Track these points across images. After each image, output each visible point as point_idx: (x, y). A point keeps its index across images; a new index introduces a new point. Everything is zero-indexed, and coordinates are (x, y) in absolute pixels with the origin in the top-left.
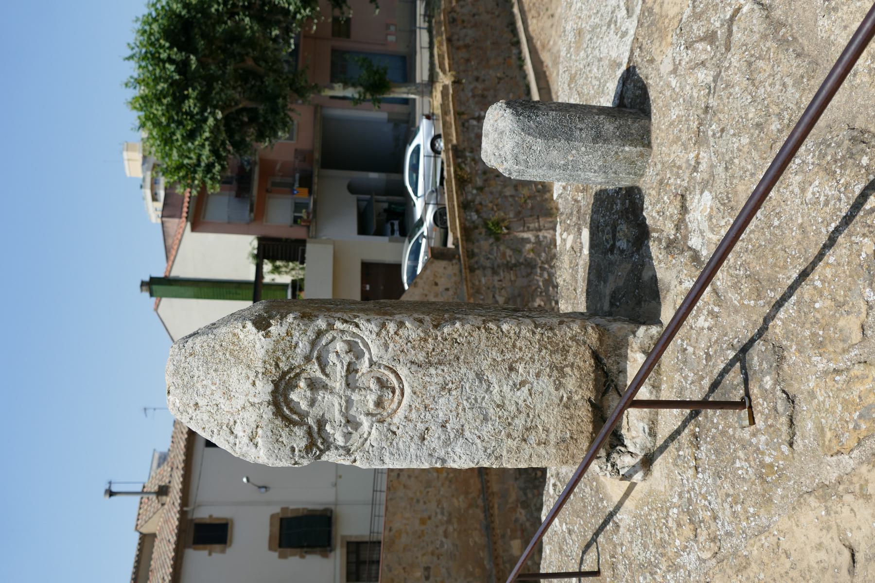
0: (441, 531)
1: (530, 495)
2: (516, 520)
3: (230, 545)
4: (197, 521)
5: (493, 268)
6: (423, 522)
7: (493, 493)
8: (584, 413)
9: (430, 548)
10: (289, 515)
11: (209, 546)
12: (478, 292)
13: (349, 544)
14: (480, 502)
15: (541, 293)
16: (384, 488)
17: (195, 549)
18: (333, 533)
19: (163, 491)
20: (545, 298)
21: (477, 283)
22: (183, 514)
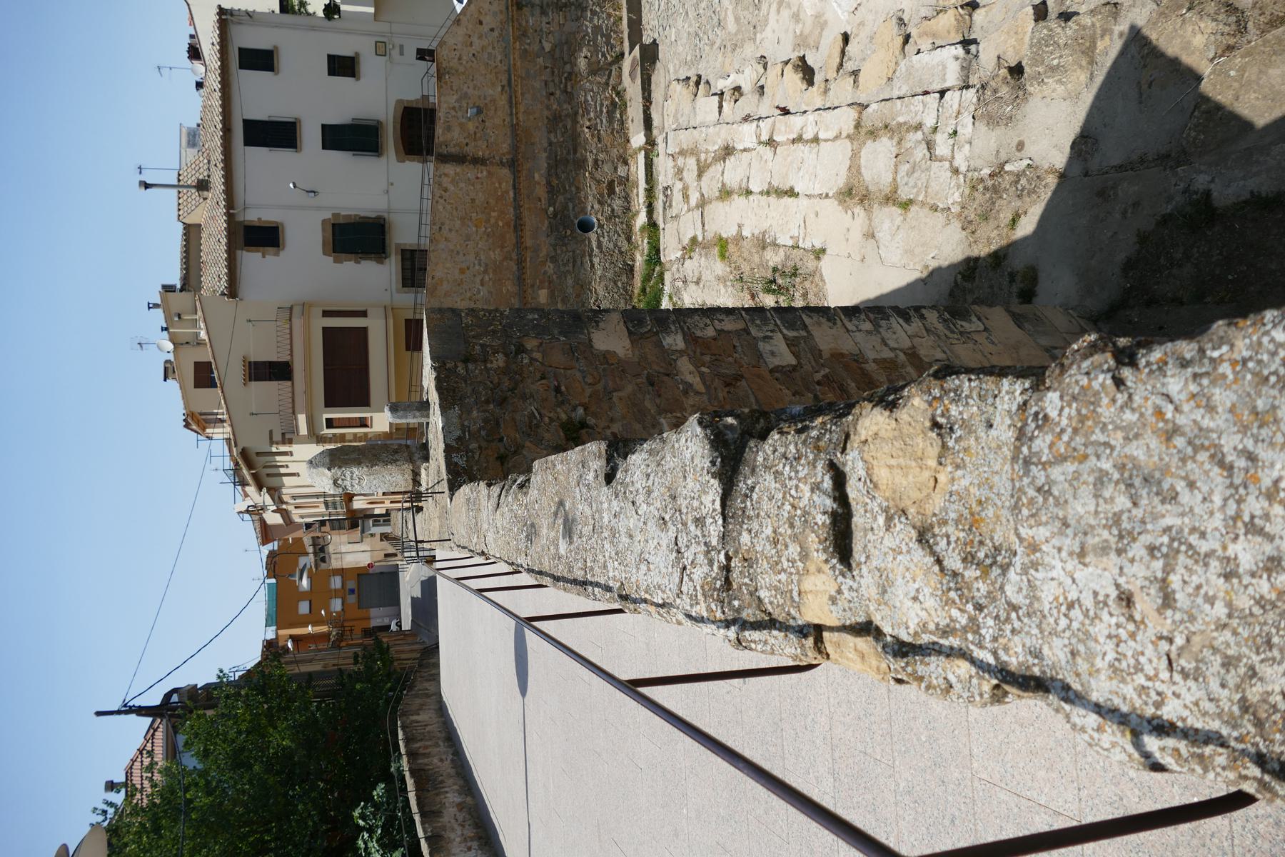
0: (478, 280)
1: (559, 252)
2: (545, 272)
3: (283, 249)
4: (246, 223)
5: (542, 7)
6: (462, 271)
7: (526, 248)
8: (411, 481)
9: (469, 294)
10: (341, 221)
11: (261, 249)
12: (524, 34)
13: (403, 251)
14: (514, 256)
15: (589, 41)
16: (429, 222)
17: (248, 251)
18: (387, 242)
19: (202, 186)
20: (592, 49)
21: (524, 23)
22: (230, 217)
